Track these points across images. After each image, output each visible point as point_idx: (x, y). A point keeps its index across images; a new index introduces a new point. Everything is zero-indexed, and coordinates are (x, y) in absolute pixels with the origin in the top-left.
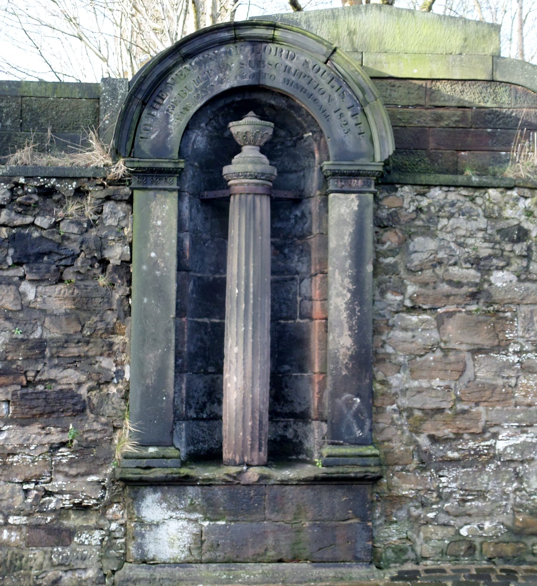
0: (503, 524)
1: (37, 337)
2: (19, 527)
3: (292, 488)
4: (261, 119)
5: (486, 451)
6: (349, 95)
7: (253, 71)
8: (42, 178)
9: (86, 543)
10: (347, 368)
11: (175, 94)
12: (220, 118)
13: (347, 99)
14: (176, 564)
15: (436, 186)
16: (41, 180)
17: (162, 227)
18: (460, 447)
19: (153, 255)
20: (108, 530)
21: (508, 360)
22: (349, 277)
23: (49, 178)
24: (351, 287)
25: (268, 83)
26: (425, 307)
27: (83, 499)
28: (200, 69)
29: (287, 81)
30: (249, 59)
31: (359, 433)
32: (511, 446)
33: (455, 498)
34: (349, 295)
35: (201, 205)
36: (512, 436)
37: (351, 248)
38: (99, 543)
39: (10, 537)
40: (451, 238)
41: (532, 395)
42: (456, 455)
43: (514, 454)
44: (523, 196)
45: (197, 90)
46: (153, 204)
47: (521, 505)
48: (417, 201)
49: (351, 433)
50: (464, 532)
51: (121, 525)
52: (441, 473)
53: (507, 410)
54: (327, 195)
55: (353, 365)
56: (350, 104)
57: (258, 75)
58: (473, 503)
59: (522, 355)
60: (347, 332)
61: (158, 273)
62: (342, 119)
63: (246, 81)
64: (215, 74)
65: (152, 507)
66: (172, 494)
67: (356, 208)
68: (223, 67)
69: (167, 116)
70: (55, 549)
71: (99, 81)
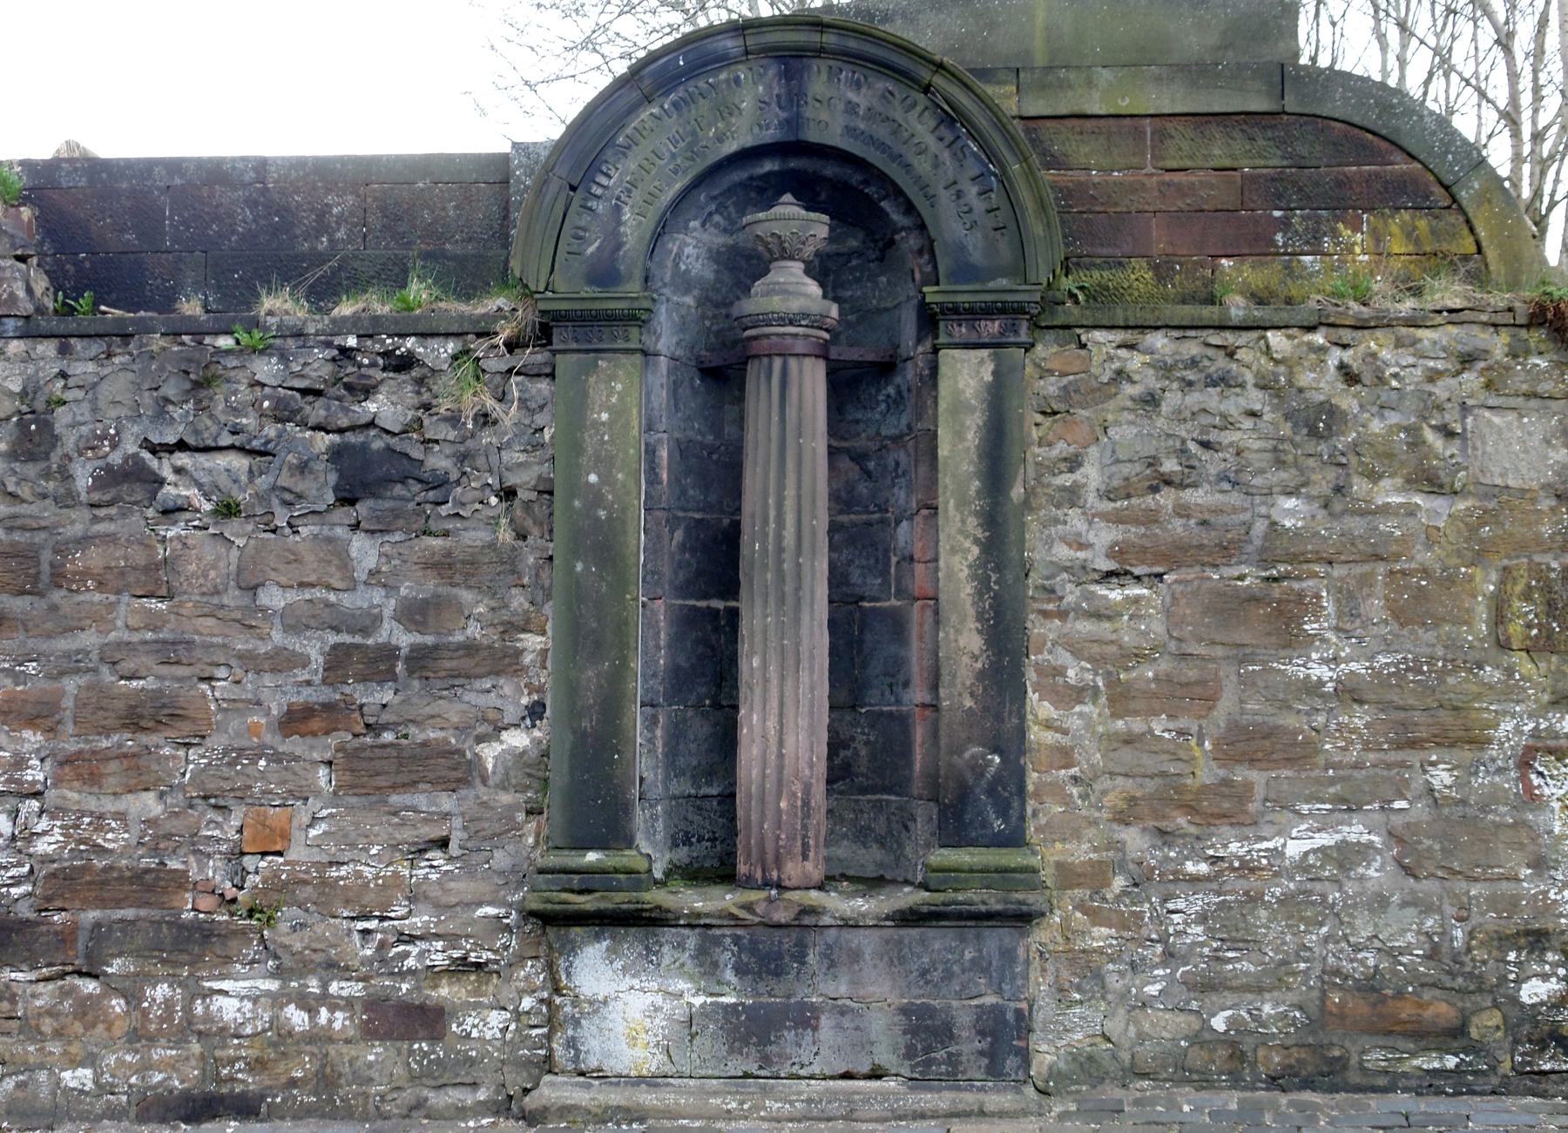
0: (1301, 1008)
1: (380, 640)
2: (349, 1003)
3: (867, 932)
4: (807, 209)
5: (1264, 861)
6: (974, 154)
7: (783, 115)
8: (389, 336)
9: (475, 1034)
10: (972, 694)
11: (633, 167)
12: (731, 209)
13: (970, 161)
14: (641, 1079)
15: (1157, 328)
16: (389, 341)
17: (610, 424)
18: (1211, 852)
19: (593, 478)
20: (516, 1010)
21: (1308, 676)
22: (976, 514)
23: (403, 336)
24: (979, 534)
25: (813, 135)
26: (1137, 571)
27: (468, 952)
28: (680, 115)
29: (850, 131)
30: (776, 92)
31: (998, 825)
32: (1315, 851)
33: (1201, 955)
34: (976, 551)
35: (702, 380)
36: (1319, 830)
37: (979, 456)
38: (499, 1035)
39: (330, 1021)
40: (1188, 432)
41: (1359, 747)
42: (1204, 868)
43: (1322, 867)
44: (1337, 344)
45: (673, 156)
46: (592, 380)
47: (1337, 972)
48: (1119, 358)
49: (985, 824)
50: (1219, 1023)
51: (542, 1001)
52: (1171, 906)
53: (1308, 777)
54: (936, 350)
55: (985, 689)
56: (976, 171)
57: (795, 122)
58: (1238, 966)
59: (1338, 665)
60: (972, 624)
61: (602, 514)
62: (962, 201)
63: (770, 135)
64: (709, 126)
65: (595, 969)
66: (632, 943)
67: (988, 378)
68: (726, 110)
69: (617, 210)
70: (416, 1046)
71: (508, 150)
